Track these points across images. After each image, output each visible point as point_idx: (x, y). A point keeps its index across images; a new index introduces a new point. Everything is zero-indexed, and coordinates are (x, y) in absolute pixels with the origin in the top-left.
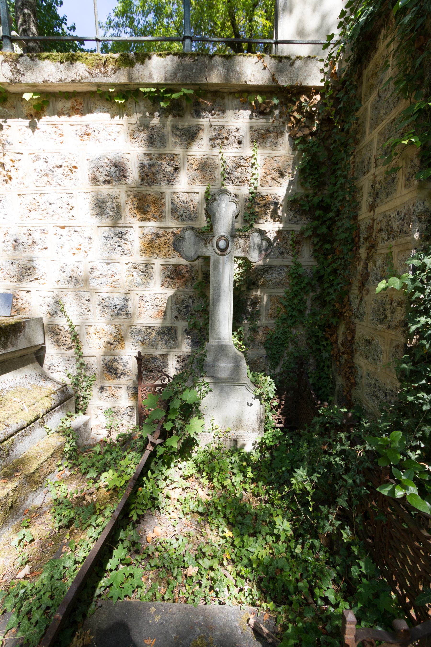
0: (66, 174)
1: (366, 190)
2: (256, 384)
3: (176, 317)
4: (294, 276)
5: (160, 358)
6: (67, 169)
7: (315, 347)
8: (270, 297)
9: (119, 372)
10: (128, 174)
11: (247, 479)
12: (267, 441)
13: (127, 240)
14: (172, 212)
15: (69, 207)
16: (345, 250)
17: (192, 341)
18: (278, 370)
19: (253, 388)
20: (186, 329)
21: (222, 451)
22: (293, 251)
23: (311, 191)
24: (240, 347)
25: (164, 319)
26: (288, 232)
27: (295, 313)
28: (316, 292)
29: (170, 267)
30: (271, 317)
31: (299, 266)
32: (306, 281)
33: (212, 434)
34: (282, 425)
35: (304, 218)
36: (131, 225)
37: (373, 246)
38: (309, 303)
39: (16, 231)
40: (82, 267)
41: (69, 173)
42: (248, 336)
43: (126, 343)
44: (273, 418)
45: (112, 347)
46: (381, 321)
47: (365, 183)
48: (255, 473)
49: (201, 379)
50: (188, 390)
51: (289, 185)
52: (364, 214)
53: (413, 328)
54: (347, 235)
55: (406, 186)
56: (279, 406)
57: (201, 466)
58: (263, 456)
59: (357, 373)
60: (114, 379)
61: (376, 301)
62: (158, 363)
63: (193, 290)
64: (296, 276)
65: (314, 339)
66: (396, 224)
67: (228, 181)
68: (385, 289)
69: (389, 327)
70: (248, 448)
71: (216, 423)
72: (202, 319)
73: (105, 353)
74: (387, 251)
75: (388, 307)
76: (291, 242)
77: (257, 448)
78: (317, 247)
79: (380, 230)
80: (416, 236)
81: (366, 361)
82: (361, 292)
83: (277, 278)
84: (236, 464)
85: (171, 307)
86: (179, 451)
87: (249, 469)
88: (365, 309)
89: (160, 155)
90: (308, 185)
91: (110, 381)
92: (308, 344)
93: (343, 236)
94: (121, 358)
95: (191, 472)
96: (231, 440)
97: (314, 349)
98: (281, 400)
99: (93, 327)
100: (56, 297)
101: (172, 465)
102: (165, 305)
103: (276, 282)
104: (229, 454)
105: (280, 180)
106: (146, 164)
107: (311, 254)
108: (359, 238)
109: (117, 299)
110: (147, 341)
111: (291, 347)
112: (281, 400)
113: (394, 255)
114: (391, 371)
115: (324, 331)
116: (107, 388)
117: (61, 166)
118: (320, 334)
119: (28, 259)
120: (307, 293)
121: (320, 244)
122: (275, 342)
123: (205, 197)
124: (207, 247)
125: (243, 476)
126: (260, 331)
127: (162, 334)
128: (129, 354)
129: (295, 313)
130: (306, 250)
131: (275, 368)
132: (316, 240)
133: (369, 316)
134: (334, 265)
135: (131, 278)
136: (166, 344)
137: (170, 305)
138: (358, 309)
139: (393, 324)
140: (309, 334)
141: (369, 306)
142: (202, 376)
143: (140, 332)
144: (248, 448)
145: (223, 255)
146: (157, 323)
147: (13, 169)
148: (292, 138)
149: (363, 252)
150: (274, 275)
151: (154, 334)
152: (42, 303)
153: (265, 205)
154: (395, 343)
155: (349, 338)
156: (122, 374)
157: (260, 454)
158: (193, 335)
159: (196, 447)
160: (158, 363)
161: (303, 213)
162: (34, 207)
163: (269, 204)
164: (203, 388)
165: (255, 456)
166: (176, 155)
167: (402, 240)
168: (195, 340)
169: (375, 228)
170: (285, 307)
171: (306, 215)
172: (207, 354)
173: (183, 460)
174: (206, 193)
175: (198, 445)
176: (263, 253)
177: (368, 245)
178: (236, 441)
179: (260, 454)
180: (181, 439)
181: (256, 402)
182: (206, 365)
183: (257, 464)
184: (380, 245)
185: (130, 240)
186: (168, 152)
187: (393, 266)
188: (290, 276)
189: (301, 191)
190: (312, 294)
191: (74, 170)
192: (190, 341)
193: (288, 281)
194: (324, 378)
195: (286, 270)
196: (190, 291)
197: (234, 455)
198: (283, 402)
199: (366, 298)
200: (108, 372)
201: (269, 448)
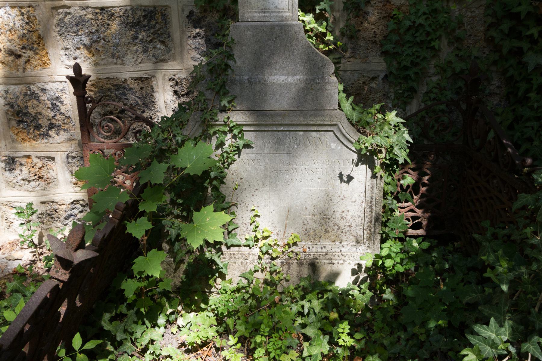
2: (361, 127)
5: (135, 86)
9: (44, 122)
11: (340, 351)
12: (389, 263)
18: (413, 108)
19: (354, 136)
20: (191, 13)
21: (279, 290)
24: (320, 37)
33: (256, 251)
34: (420, 232)
42: (342, 25)
43: (51, 51)
44: (403, 212)
45: (22, 61)
48: (358, 336)
49: (222, 117)
50: (190, 144)
56: (415, 188)
57: (230, 322)
58: (377, 298)
60: (35, 138)
62: (132, 98)
70: (344, 282)
71: (265, 224)
73: (6, 77)
77: (364, 281)
84: (312, 317)
86: (178, 290)
87: (345, 327)
91: (27, 144)
92: (490, 40)
94: (44, 90)
95: (203, 334)
96: (300, 263)
97: (505, 51)
98: (422, 174)
101: (161, 320)
104: (297, 294)
110: (99, 46)
111: (446, 52)
112: (422, 174)
122: (408, 37)
125: (330, 343)
126: (370, 10)
131: (405, 103)
136: (145, 51)
142: (224, 110)
143: (80, 22)
144: (344, 282)
151: (115, 27)
156: (51, 126)
157: (369, 294)
158: (208, 28)
159: (219, 280)
160: (132, 98)
164: (229, 141)
165: (361, 297)
172: (236, 52)
173: (188, 309)
175: (223, 276)
178: (314, 266)
179: (369, 294)
180: (182, 261)
181: (362, 172)
182: (233, 82)
183: (363, 315)
192: (202, 41)
194: (528, 120)
197: (309, 297)
198: (425, 179)
200: (19, 122)
201: (394, 280)
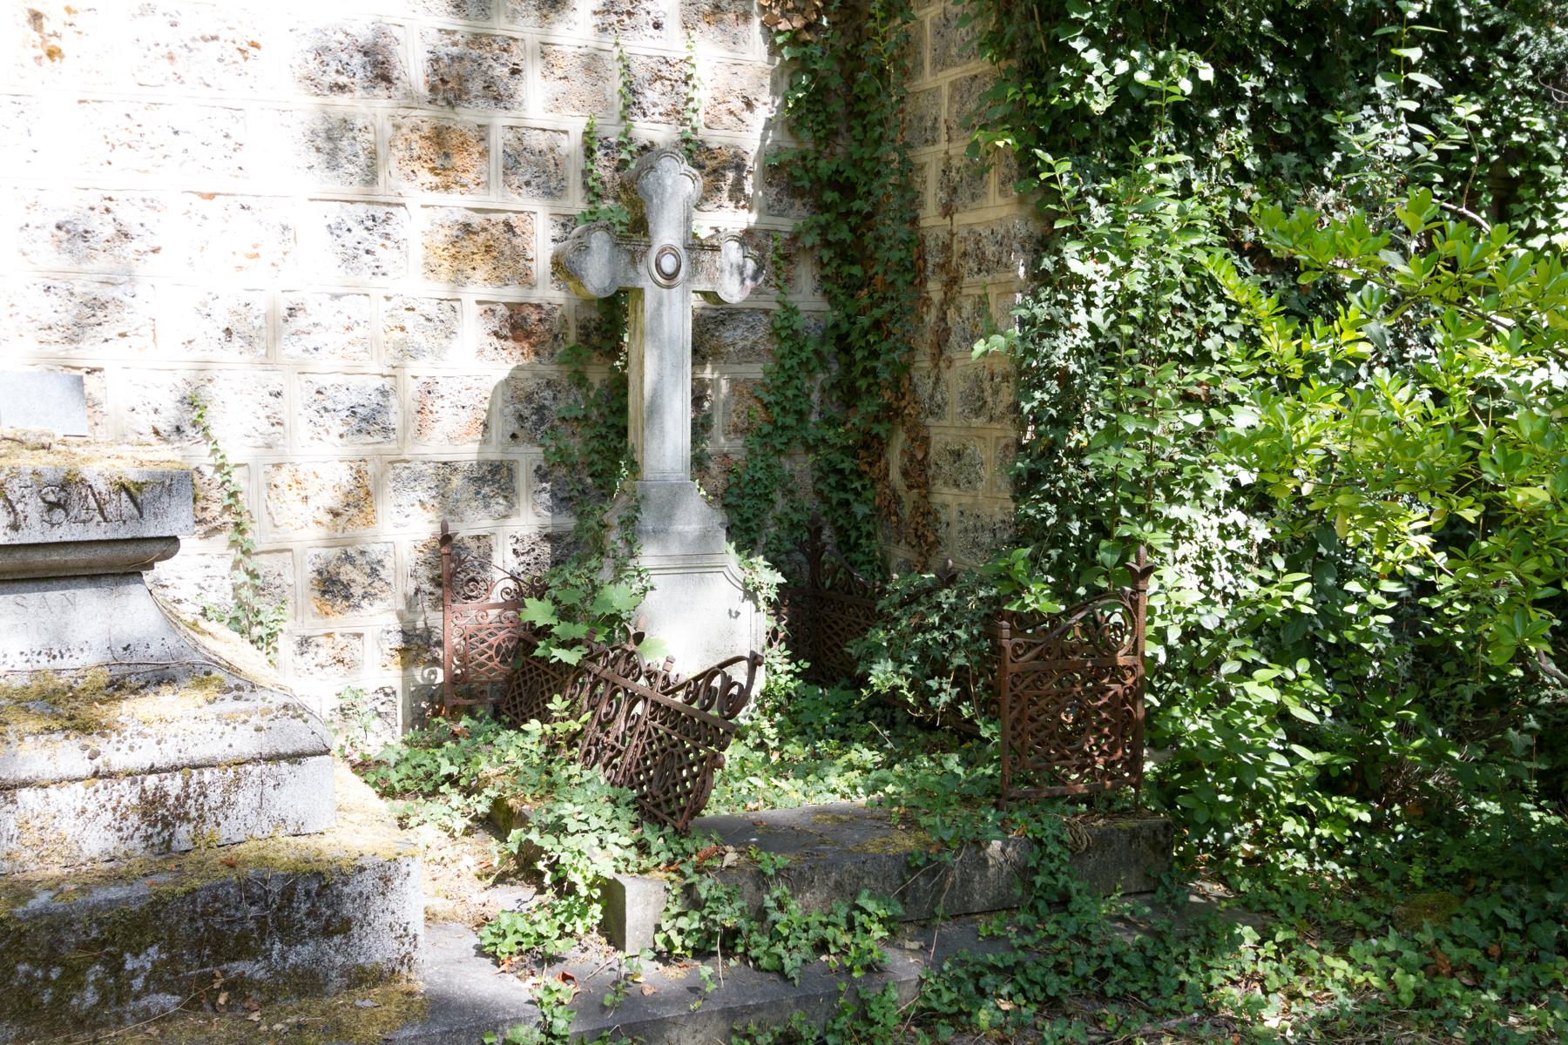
0: (228, 60)
1: (932, 174)
3: (514, 436)
4: (783, 334)
6: (232, 48)
7: (836, 497)
8: (734, 382)
10: (395, 74)
13: (387, 236)
14: (505, 174)
15: (231, 143)
16: (900, 283)
17: (553, 495)
20: (539, 467)
22: (778, 276)
23: (810, 146)
25: (484, 442)
26: (768, 233)
27: (790, 420)
28: (829, 370)
29: (502, 310)
30: (735, 431)
31: (791, 311)
32: (810, 346)
35: (798, 203)
36: (401, 200)
37: (953, 282)
38: (815, 397)
39: (66, 203)
40: (261, 304)
41: (238, 57)
45: (341, 521)
46: (977, 413)
47: (931, 158)
51: (766, 128)
52: (930, 217)
53: (1027, 408)
54: (903, 254)
55: (1003, 193)
59: (937, 520)
61: (965, 378)
63: (555, 367)
64: (786, 332)
65: (832, 480)
66: (990, 250)
67: (635, 110)
68: (985, 353)
69: (991, 419)
72: (577, 439)
74: (981, 292)
75: (987, 385)
76: (775, 258)
78: (828, 271)
79: (965, 254)
80: (1022, 270)
81: (956, 491)
82: (936, 365)
83: (746, 338)
85: (502, 412)
88: (946, 396)
89: (477, 36)
90: (806, 135)
92: (819, 493)
93: (896, 255)
97: (834, 502)
99: (285, 469)
100: (181, 385)
102: (487, 406)
103: (743, 349)
105: (746, 115)
106: (442, 54)
107: (816, 284)
108: (925, 261)
109: (363, 390)
111: (781, 504)
113: (992, 299)
114: (999, 490)
115: (856, 456)
116: (321, 640)
117: (214, 38)
118: (847, 465)
119: (102, 277)
120: (810, 373)
121: (834, 265)
122: (747, 490)
123: (585, 142)
124: (635, 269)
127: (476, 480)
128: (404, 530)
129: (790, 420)
130: (805, 276)
132: (827, 255)
133: (955, 407)
134: (877, 313)
135: (398, 335)
137: (500, 404)
138: (932, 397)
139: (997, 412)
140: (821, 469)
141: (955, 384)
145: (669, 287)
146: (468, 452)
147: (68, 33)
148: (769, 30)
149: (934, 289)
150: (739, 331)
152: (136, 403)
153: (715, 171)
154: (1003, 442)
155: (920, 456)
158: (556, 482)
161: (796, 192)
162: (125, 137)
163: (724, 168)
166: (515, 40)
167: (1002, 277)
168: (560, 495)
169: (955, 247)
170: (766, 406)
171: (802, 196)
174: (585, 133)
176: (749, 283)
177: (944, 277)
184: (967, 280)
185: (395, 236)
186: (498, 32)
187: (990, 317)
188: (775, 333)
189: (789, 144)
190: (821, 376)
191: (253, 51)
193: (769, 346)
195: (765, 320)
196: (550, 370)
199: (947, 375)
